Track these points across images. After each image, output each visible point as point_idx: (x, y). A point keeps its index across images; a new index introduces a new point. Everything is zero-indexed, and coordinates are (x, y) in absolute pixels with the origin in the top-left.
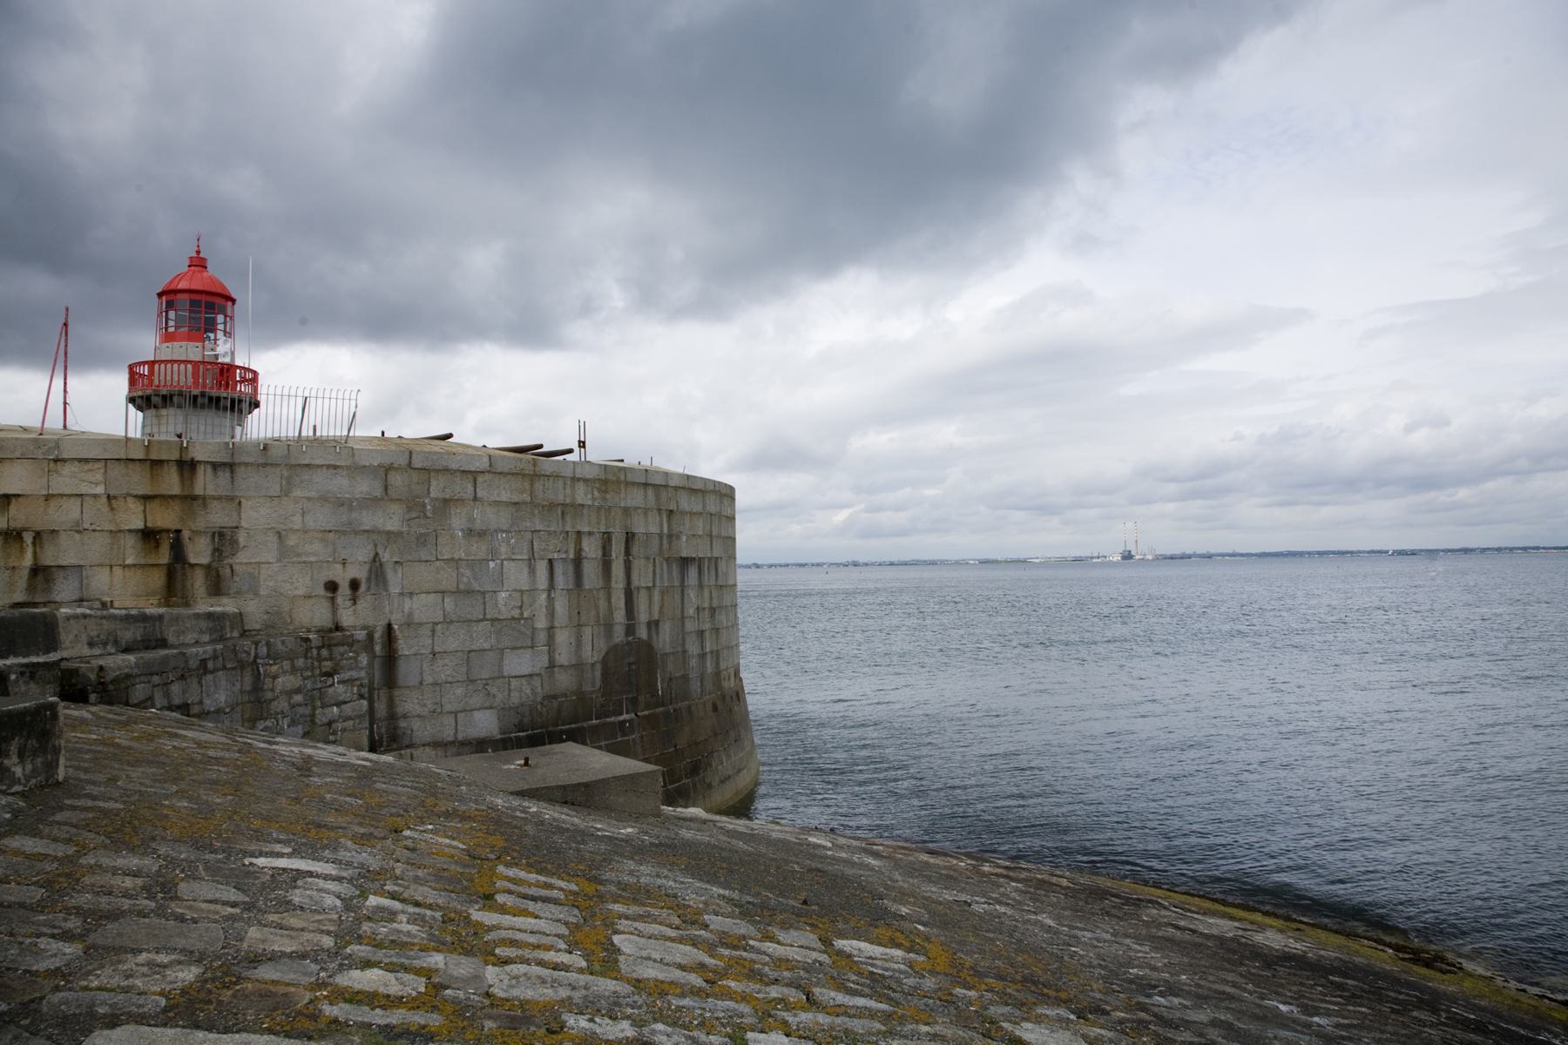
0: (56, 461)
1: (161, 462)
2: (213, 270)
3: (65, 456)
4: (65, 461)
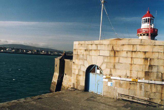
0: (154, 45)
4: (156, 45)
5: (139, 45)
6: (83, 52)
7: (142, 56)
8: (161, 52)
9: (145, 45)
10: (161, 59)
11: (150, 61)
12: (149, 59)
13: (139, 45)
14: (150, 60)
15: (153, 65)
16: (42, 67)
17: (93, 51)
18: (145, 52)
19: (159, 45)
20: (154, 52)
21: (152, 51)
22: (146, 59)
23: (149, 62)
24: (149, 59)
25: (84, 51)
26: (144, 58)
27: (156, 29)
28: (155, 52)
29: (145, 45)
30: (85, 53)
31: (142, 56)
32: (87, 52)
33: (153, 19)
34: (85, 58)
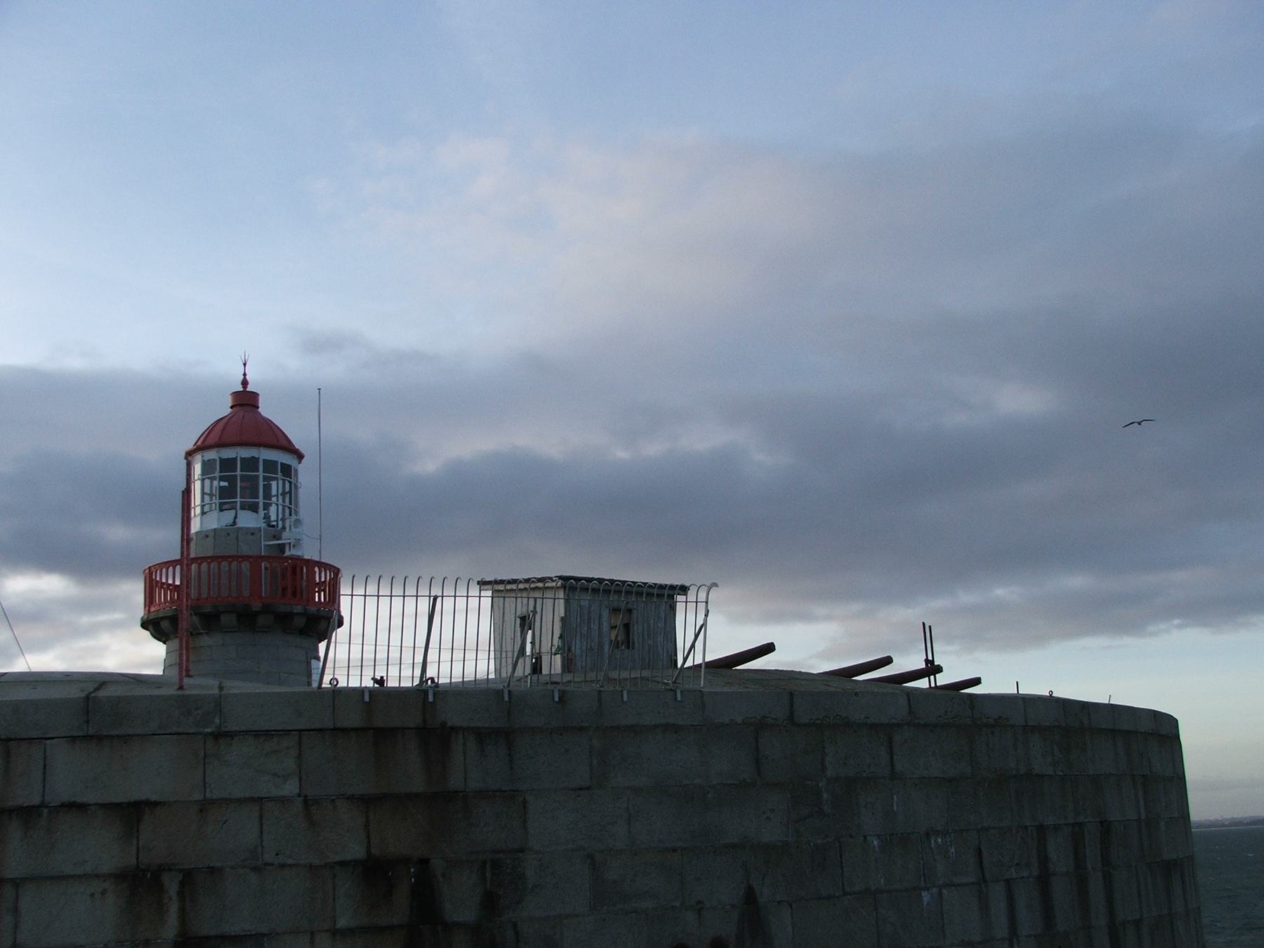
0: (218, 735)
1: (393, 731)
2: (265, 410)
3: (232, 726)
4: (231, 735)
5: (73, 739)
7: (100, 849)
8: (283, 801)
9: (126, 739)
10: (282, 866)
11: (181, 894)
12: (172, 885)
13: (73, 739)
14: (182, 884)
15: (213, 933)
16: (926, 897)
18: (131, 814)
19: (257, 734)
20: (213, 802)
21: (198, 796)
22: (140, 883)
23: (173, 909)
24: (172, 885)
26: (120, 876)
27: (162, 618)
28: (228, 801)
29: (126, 739)
31: (100, 849)
33: (287, 470)
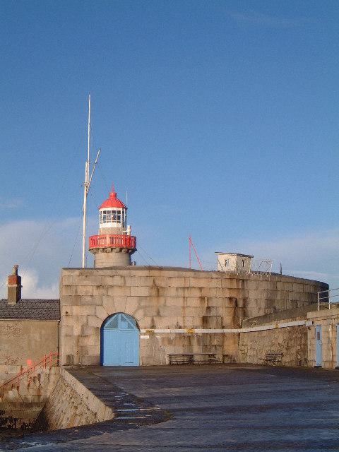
6: (91, 290)
17: (116, 289)
25: (95, 288)
30: (96, 293)
32: (102, 291)
34: (98, 302)
